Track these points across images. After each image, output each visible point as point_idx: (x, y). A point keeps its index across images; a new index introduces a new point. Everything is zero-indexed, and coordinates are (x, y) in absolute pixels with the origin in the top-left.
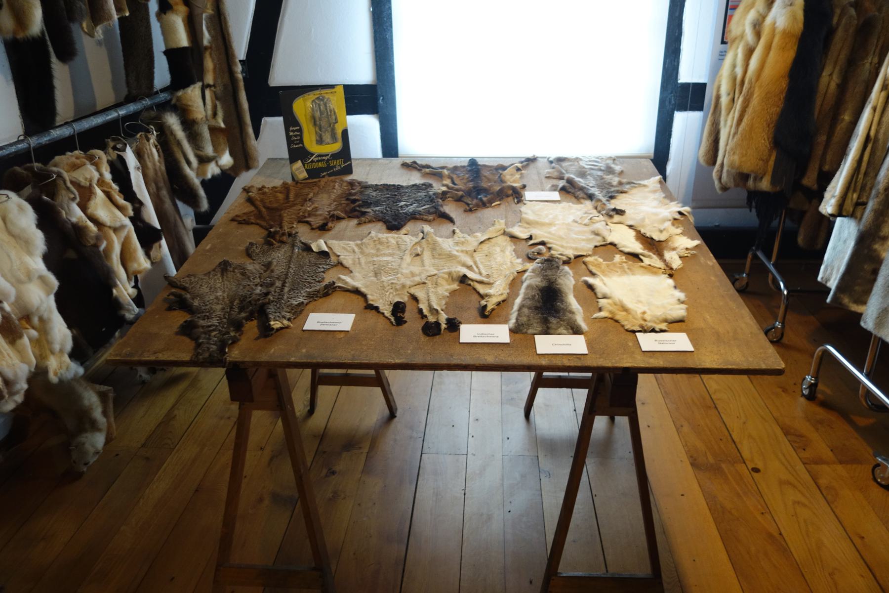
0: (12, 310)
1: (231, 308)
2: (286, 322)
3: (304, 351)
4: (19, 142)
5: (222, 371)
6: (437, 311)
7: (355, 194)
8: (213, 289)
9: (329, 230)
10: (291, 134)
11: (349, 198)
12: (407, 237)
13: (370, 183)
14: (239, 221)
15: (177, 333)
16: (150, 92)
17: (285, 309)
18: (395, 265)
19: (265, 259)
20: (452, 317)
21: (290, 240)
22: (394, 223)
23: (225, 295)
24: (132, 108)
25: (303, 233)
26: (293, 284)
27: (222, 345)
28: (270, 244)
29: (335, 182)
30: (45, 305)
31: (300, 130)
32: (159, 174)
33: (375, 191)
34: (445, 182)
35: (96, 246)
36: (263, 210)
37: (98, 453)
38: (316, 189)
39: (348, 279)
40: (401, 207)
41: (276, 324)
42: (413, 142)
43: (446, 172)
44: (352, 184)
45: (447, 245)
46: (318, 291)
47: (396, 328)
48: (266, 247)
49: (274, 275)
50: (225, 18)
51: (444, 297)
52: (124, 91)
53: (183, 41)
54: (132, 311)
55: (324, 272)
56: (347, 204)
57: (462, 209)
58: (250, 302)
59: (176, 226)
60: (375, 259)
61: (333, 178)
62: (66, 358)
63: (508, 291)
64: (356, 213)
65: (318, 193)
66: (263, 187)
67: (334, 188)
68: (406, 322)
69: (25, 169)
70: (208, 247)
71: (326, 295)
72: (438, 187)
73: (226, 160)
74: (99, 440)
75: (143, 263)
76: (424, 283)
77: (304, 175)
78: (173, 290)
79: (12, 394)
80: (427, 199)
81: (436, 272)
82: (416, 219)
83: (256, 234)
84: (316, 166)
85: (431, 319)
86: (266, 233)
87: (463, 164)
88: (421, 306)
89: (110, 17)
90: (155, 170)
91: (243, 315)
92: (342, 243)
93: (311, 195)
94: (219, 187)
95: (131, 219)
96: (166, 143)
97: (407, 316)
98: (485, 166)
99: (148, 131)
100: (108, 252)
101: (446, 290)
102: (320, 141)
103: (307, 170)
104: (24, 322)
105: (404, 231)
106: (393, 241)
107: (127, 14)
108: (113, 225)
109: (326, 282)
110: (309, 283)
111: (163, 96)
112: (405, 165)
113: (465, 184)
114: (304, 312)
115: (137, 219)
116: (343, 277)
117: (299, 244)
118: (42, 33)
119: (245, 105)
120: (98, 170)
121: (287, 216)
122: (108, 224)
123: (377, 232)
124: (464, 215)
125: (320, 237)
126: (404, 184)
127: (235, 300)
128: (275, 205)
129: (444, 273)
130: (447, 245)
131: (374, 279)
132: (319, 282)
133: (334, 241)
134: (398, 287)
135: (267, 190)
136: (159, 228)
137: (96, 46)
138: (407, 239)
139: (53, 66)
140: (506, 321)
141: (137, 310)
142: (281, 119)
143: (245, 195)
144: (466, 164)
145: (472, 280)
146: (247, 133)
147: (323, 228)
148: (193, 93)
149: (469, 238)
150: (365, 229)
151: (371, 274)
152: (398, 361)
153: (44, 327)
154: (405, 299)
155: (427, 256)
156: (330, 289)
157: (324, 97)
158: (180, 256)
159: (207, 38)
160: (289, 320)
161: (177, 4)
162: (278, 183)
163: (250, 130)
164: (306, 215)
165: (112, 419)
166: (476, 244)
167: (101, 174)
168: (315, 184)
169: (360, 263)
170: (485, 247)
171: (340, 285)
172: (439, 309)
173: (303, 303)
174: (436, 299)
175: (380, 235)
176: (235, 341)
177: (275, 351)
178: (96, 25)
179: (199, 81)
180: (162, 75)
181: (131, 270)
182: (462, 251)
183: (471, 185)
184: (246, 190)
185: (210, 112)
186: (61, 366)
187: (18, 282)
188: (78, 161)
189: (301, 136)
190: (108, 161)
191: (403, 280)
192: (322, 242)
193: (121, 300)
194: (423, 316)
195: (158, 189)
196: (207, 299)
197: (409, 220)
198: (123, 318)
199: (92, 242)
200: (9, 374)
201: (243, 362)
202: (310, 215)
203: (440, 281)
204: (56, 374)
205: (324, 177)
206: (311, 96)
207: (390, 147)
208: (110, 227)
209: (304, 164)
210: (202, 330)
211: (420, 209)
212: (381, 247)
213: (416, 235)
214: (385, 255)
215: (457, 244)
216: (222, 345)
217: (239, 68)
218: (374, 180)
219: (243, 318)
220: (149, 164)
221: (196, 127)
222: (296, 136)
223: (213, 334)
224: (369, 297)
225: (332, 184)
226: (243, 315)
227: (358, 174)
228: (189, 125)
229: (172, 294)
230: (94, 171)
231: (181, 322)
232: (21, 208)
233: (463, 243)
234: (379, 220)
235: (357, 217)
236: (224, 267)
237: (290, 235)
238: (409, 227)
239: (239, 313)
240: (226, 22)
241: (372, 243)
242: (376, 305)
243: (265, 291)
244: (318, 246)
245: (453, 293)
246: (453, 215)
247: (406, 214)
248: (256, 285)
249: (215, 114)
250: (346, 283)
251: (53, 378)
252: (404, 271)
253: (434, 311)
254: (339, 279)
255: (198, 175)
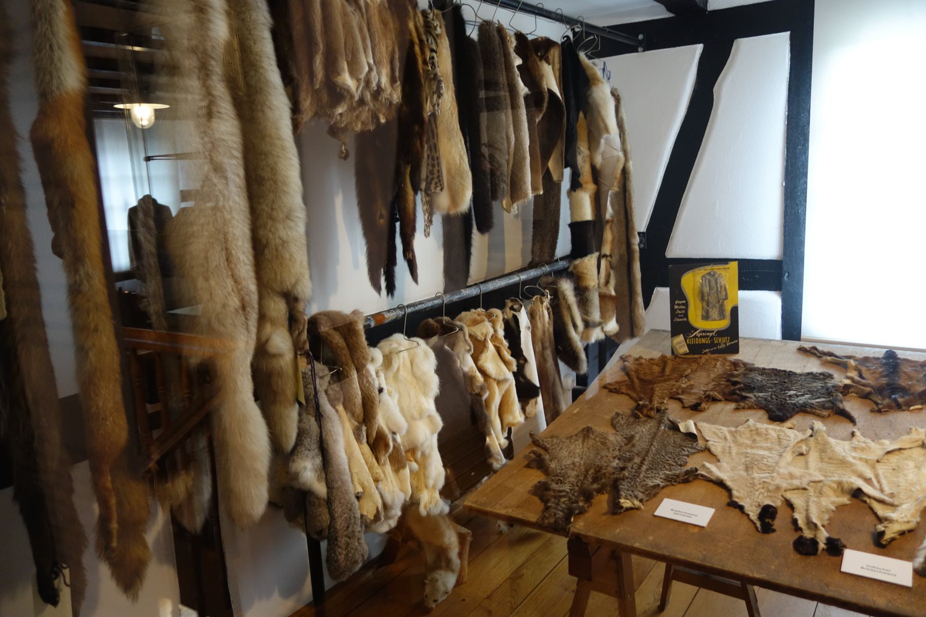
0: (403, 442)
1: (585, 477)
2: (637, 503)
3: (651, 538)
4: (437, 298)
5: (565, 540)
6: (815, 525)
7: (737, 376)
8: (571, 454)
9: (701, 411)
10: (676, 307)
11: (729, 379)
12: (792, 432)
13: (756, 366)
14: (610, 389)
15: (530, 492)
16: (551, 260)
17: (639, 488)
18: (771, 462)
19: (628, 432)
20: (835, 536)
21: (658, 416)
22: (778, 413)
23: (582, 462)
24: (533, 273)
25: (673, 411)
26: (653, 462)
27: (569, 513)
28: (636, 417)
29: (717, 360)
30: (428, 443)
31: (686, 305)
32: (547, 335)
33: (762, 375)
34: (849, 374)
35: (479, 395)
36: (636, 381)
37: (447, 593)
38: (695, 366)
39: (713, 468)
40: (790, 396)
41: (626, 503)
42: (816, 324)
43: (852, 362)
44: (735, 364)
45: (841, 447)
46: (678, 476)
47: (759, 535)
48: (632, 419)
49: (635, 450)
50: (630, 194)
51: (828, 511)
52: (529, 258)
53: (587, 214)
54: (499, 461)
55: (688, 456)
56: (727, 386)
57: (869, 409)
58: (604, 474)
59: (554, 384)
60: (749, 451)
61: (715, 356)
62: (437, 495)
63: (918, 519)
64: (736, 397)
65: (696, 370)
66: (641, 358)
67: (715, 367)
68: (774, 531)
69: (436, 321)
70: (575, 411)
71: (686, 481)
72: (840, 379)
73: (612, 326)
74: (448, 580)
75: (517, 416)
76: (805, 489)
77: (685, 349)
78: (535, 449)
79: (387, 518)
80: (824, 391)
81: (822, 478)
82: (806, 412)
83: (624, 405)
84: (698, 341)
85: (808, 534)
86: (634, 404)
87: (877, 356)
88: (797, 515)
89: (526, 195)
90: (544, 331)
91: (595, 486)
92: (713, 427)
93: (689, 371)
94: (606, 347)
95: (514, 373)
96: (557, 308)
97: (777, 523)
98: (907, 360)
99: (543, 295)
100: (488, 402)
101: (833, 503)
102: (706, 317)
103: (688, 345)
104: (409, 454)
105: (788, 424)
106: (773, 434)
107: (541, 193)
108: (497, 378)
109: (688, 467)
110: (670, 465)
111: (562, 264)
112: (802, 350)
113: (877, 379)
114: (659, 495)
115: (520, 375)
116: (708, 465)
117: (667, 422)
118: (470, 210)
119: (638, 274)
120: (494, 327)
121: (659, 390)
122: (494, 376)
123: (756, 421)
124: (870, 416)
125: (690, 417)
126: (798, 371)
127: (590, 469)
128: (649, 378)
129: (832, 481)
130: (841, 447)
131: (744, 473)
132: (681, 465)
133: (705, 424)
134: (771, 488)
135: (643, 361)
136: (538, 385)
137: (513, 218)
138: (791, 433)
139: (473, 236)
140: (910, 558)
141: (504, 460)
142: (667, 290)
143: (621, 363)
144: (881, 356)
145: (869, 497)
146: (636, 302)
147: (696, 408)
148: (589, 263)
149: (872, 445)
150: (742, 415)
151: (742, 467)
152: (757, 575)
153: (423, 463)
154: (777, 503)
155: (813, 457)
156: (691, 476)
157: (715, 273)
158: (553, 412)
159: (609, 212)
160: (641, 501)
161: (587, 183)
162: (656, 355)
163: (640, 300)
164: (680, 391)
165: (466, 563)
166: (881, 453)
167: (495, 331)
168: (695, 360)
169: (730, 453)
170: (893, 458)
171: (704, 473)
172: (819, 524)
173: (659, 485)
174: (817, 510)
175: (759, 425)
176: (582, 512)
177: (618, 532)
178: (513, 203)
179: (597, 251)
180: (564, 244)
181: (506, 421)
182: (861, 459)
183: (884, 381)
184: (623, 359)
185: (603, 280)
186: (432, 502)
187: (410, 419)
188: (479, 318)
189: (686, 310)
190: (504, 319)
191: (778, 481)
192: (691, 423)
193: (492, 449)
194: (798, 529)
195: (544, 348)
196: (564, 463)
197: (797, 413)
198: (490, 466)
199: (477, 391)
200: (389, 499)
201: (586, 536)
202: (683, 393)
203: (826, 490)
204: (425, 507)
205: (706, 353)
206: (702, 271)
207: (791, 327)
208: (494, 379)
209: (686, 339)
210: (552, 493)
211: (813, 401)
212: (758, 439)
213: (803, 431)
214: (761, 448)
215: (855, 449)
216: (569, 513)
217: (636, 240)
218: (762, 362)
219: (595, 490)
220: (539, 325)
221: (587, 293)
222: (680, 310)
223: (562, 500)
224: (735, 493)
225: (713, 362)
226: (595, 486)
227: (745, 355)
228: (581, 292)
229: (533, 452)
230: (490, 327)
231: (536, 482)
232: (426, 354)
233: (863, 449)
234: (761, 408)
235: (736, 401)
236: (587, 432)
237: (658, 410)
238: (796, 420)
239: (592, 483)
240: (630, 199)
241: (748, 432)
242: (741, 503)
243: (621, 466)
244: (687, 427)
245: (840, 508)
246: (854, 414)
247: (794, 404)
248: (614, 458)
249: (607, 282)
250: (710, 472)
251: (423, 511)
252: (782, 471)
253: (813, 526)
254: (704, 466)
255: (582, 339)
